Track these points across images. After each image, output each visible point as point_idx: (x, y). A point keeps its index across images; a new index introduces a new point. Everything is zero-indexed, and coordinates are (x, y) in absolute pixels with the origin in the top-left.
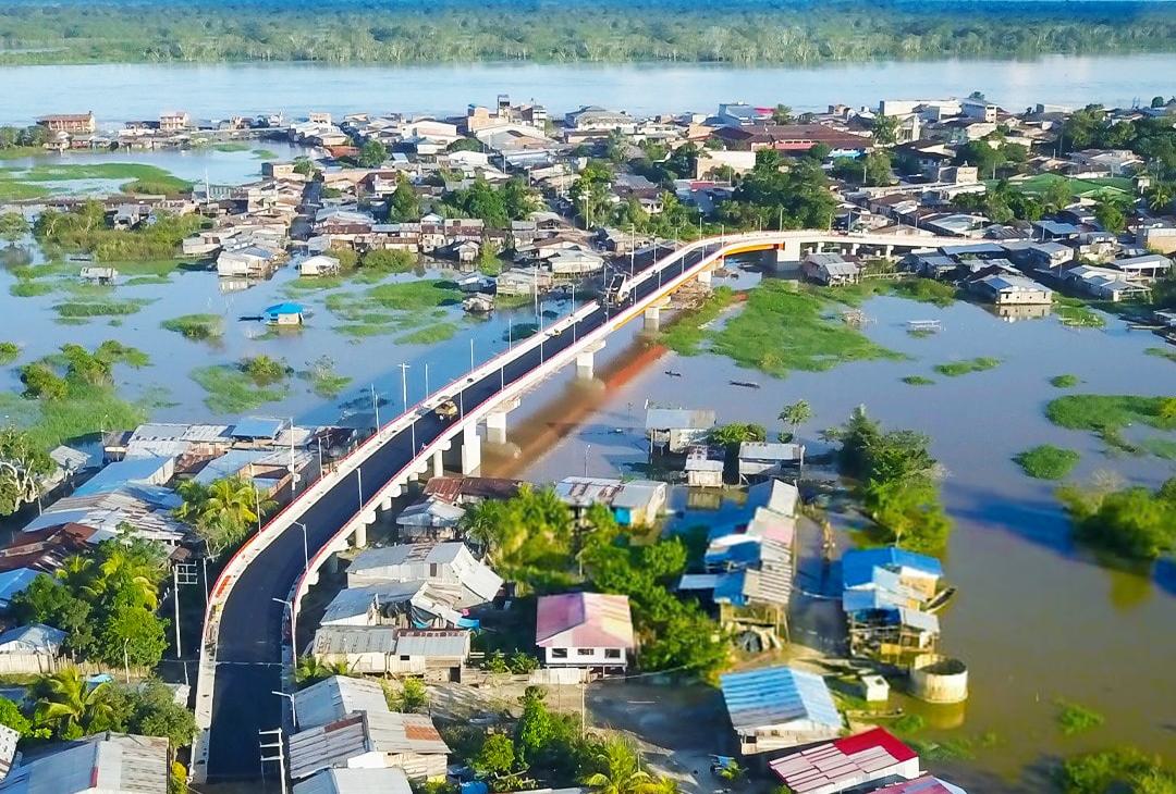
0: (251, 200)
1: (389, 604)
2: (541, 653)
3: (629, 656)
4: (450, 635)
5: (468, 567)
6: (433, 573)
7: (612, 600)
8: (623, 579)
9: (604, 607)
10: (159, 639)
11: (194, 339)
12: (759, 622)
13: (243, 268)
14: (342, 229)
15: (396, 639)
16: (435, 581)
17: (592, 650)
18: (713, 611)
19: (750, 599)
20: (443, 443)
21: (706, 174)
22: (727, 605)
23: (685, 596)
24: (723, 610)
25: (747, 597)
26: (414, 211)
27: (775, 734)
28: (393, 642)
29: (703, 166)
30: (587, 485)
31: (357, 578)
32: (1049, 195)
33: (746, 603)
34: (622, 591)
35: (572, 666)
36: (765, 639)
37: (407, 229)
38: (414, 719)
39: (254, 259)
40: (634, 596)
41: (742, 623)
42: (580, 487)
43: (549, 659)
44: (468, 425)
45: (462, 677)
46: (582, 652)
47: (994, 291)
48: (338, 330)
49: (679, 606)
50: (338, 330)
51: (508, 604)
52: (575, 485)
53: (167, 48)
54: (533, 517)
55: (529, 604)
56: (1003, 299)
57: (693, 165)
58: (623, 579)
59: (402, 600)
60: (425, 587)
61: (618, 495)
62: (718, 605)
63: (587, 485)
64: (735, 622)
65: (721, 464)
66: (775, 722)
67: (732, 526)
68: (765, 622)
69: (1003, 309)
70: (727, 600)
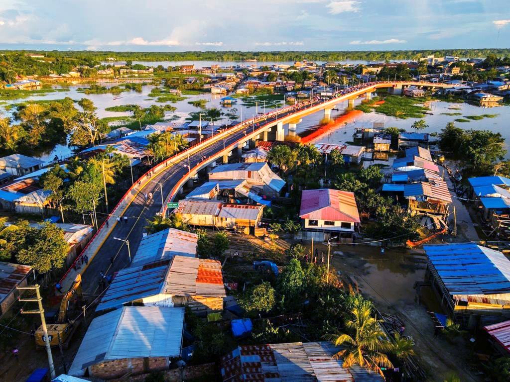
0: (227, 78)
1: (224, 190)
2: (302, 222)
3: (355, 227)
4: (251, 208)
5: (268, 175)
6: (249, 176)
7: (347, 195)
8: (351, 184)
9: (340, 197)
10: (397, 276)
11: (197, 106)
12: (433, 211)
13: (218, 91)
14: (252, 83)
15: (220, 208)
16: (250, 180)
17: (334, 222)
18: (404, 203)
19: (428, 198)
20: (267, 129)
21: (366, 73)
22: (413, 201)
23: (385, 194)
24: (410, 203)
25: (426, 197)
26: (275, 78)
27: (485, 301)
28: (218, 209)
29: (365, 71)
30: (329, 146)
31: (214, 176)
32: (286, 261)
33: (426, 200)
34: (351, 190)
35: (321, 231)
36: (436, 222)
37: (271, 83)
38: (209, 264)
39: (223, 89)
40: (357, 194)
41: (420, 212)
42: (326, 146)
43: (307, 226)
44: (280, 124)
45: (255, 232)
46: (326, 223)
47: (479, 98)
48: (243, 105)
49: (382, 200)
50: (243, 105)
51: (287, 194)
52: (324, 145)
53: (220, 57)
54: (303, 156)
55: (297, 195)
56: (483, 100)
57: (361, 71)
58: (351, 184)
59: (230, 188)
60: (244, 183)
61: (344, 150)
62: (408, 200)
63: (329, 146)
64: (417, 211)
65: (390, 141)
66: (486, 292)
67: (406, 163)
68: (436, 212)
69: (483, 103)
70: (414, 198)
